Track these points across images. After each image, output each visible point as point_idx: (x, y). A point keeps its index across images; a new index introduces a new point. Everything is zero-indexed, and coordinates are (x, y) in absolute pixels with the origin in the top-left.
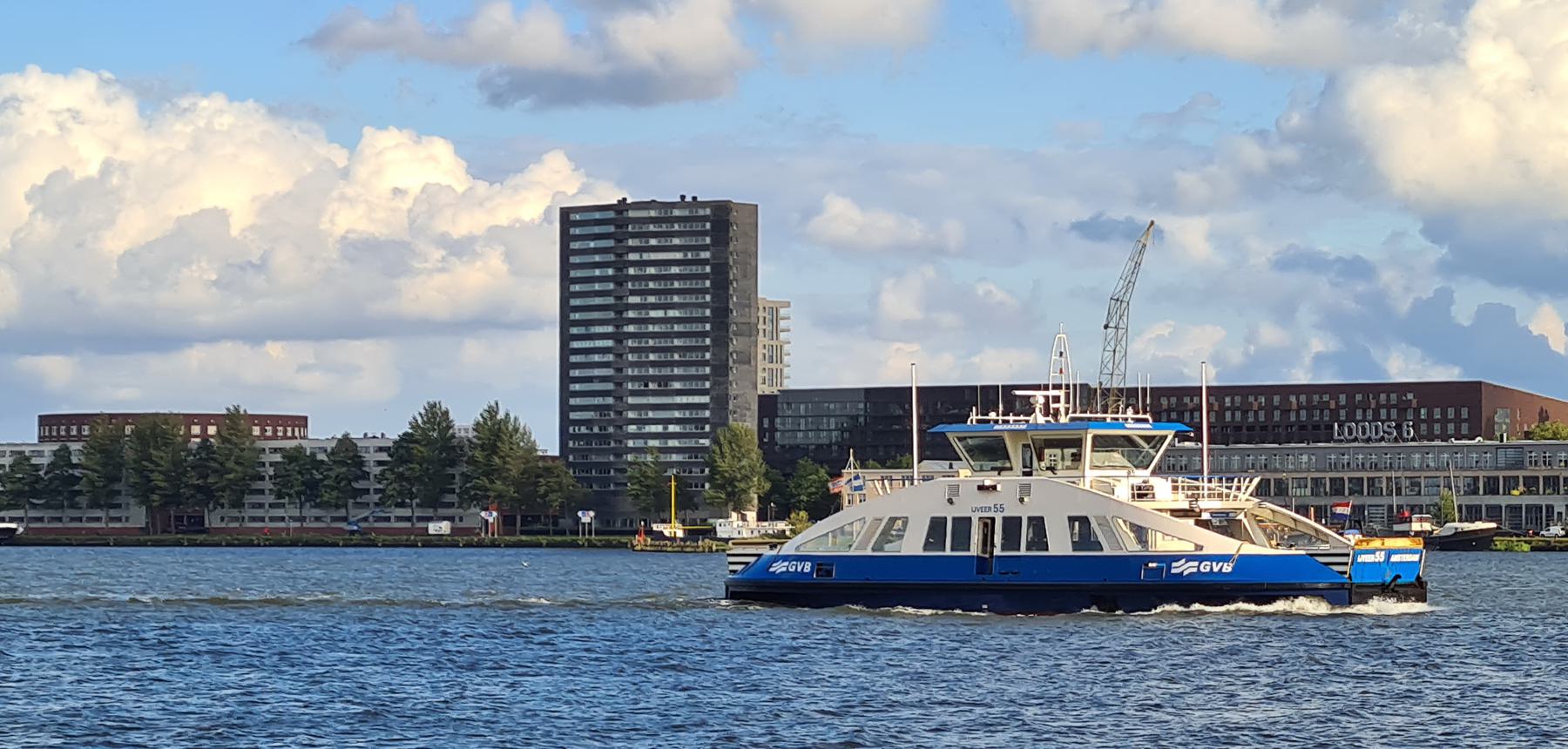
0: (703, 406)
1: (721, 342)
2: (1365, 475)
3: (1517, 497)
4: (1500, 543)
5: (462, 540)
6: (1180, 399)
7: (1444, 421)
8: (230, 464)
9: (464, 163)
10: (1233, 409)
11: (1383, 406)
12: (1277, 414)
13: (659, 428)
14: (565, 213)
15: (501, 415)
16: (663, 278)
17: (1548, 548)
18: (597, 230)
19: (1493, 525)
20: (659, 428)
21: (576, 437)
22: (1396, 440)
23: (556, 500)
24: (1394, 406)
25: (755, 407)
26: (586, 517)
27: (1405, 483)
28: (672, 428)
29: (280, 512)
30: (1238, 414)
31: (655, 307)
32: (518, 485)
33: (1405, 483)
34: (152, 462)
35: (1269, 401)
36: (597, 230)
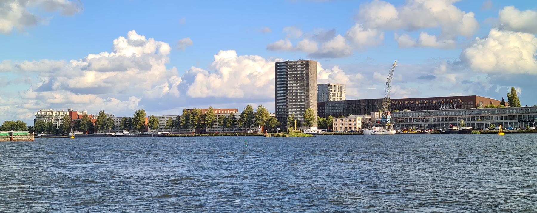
0: (304, 105)
1: (308, 91)
2: (445, 117)
3: (479, 121)
4: (473, 132)
5: (254, 134)
6: (446, 100)
7: (464, 105)
10: (421, 103)
16: (291, 76)
17: (484, 133)
18: (282, 67)
21: (279, 112)
23: (273, 125)
25: (316, 105)
26: (279, 129)
27: (454, 118)
28: (298, 110)
29: (220, 129)
31: (294, 84)
32: (266, 122)
33: (454, 118)
36: (282, 67)
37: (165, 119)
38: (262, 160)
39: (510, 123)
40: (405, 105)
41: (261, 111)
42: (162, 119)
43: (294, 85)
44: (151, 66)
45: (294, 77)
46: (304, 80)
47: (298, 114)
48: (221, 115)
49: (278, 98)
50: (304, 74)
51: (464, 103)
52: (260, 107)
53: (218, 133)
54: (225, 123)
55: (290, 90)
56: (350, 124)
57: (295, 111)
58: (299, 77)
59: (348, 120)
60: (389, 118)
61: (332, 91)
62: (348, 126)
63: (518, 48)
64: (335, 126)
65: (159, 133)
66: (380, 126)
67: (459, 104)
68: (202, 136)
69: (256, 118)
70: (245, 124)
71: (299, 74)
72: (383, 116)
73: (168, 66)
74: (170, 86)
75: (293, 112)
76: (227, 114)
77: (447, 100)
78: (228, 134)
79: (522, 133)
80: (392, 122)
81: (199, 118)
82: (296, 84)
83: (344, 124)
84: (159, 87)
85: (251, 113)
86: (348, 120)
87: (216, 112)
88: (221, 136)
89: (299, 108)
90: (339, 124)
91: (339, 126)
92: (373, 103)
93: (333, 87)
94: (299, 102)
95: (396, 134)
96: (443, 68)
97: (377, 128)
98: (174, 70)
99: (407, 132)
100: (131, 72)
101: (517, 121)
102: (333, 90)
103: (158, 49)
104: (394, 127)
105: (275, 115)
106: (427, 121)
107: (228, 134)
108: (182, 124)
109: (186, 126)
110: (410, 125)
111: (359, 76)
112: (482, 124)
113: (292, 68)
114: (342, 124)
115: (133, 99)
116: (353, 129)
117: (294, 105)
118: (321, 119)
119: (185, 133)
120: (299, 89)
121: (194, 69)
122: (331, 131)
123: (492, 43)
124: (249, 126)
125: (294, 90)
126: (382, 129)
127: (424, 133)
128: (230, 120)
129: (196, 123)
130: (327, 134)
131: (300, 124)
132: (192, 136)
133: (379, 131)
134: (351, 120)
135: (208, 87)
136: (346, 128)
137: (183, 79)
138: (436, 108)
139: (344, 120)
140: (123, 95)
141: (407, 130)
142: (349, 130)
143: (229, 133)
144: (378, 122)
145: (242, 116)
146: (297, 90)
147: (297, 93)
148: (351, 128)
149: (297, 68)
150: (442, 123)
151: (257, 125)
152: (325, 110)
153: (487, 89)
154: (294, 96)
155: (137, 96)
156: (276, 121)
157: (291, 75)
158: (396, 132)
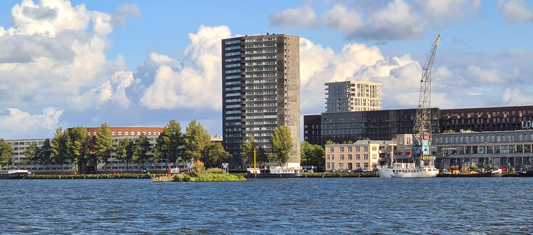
1: (281, 93)
8: (102, 146)
10: (496, 118)
11: (495, 117)
12: (514, 119)
13: (258, 129)
14: (224, 41)
15: (197, 125)
16: (253, 66)
18: (235, 48)
20: (258, 129)
21: (229, 133)
28: (263, 129)
29: (122, 165)
30: (498, 119)
31: (256, 79)
32: (202, 152)
34: (75, 146)
36: (235, 48)
37: (25, 146)
38: (113, 231)
40: (466, 120)
41: (194, 132)
42: (19, 146)
43: (256, 82)
44: (74, 54)
45: (255, 67)
46: (274, 72)
47: (263, 138)
48: (124, 138)
49: (227, 107)
50: (274, 60)
52: (193, 123)
53: (117, 172)
54: (130, 153)
55: (248, 91)
56: (358, 157)
57: (257, 132)
58: (265, 66)
59: (354, 148)
60: (426, 144)
61: (354, 95)
62: (354, 162)
64: (330, 161)
65: (10, 172)
68: (87, 178)
69: (186, 144)
70: (165, 156)
71: (265, 60)
72: (415, 141)
73: (110, 54)
74: (114, 87)
75: (253, 133)
76: (134, 136)
78: (134, 175)
80: (434, 153)
81: (83, 145)
82: (260, 79)
84: (96, 90)
85: (178, 134)
86: (354, 148)
87: (120, 133)
88: (122, 178)
89: (265, 126)
90: (336, 156)
92: (409, 118)
94: (266, 114)
95: (438, 176)
97: (403, 165)
98: (120, 60)
99: (457, 172)
100: (43, 63)
102: (356, 92)
103: (91, 23)
104: (438, 164)
105: (221, 139)
106: (498, 152)
107: (134, 175)
108: (52, 155)
109: (60, 160)
110: (467, 160)
113: (251, 50)
114: (343, 157)
115: (50, 111)
116: (362, 166)
117: (257, 120)
118: (312, 147)
119: (59, 173)
120: (265, 90)
121: (156, 57)
122: (323, 170)
124: (173, 160)
125: (256, 91)
126: (412, 166)
127: (489, 175)
128: (140, 148)
129: (78, 153)
130: (316, 177)
131: (266, 157)
132: (70, 178)
133: (406, 171)
135: (178, 92)
136: (350, 165)
137: (135, 77)
139: (346, 149)
140: (31, 103)
141: (460, 169)
142: (355, 168)
143: (136, 172)
144: (408, 153)
145: (160, 141)
146: (260, 91)
147: (262, 97)
148: (358, 165)
149: (261, 49)
150: (526, 155)
151: (187, 158)
152: (320, 129)
154: (256, 103)
155: (57, 106)
156: (221, 150)
157: (250, 62)
158: (437, 172)
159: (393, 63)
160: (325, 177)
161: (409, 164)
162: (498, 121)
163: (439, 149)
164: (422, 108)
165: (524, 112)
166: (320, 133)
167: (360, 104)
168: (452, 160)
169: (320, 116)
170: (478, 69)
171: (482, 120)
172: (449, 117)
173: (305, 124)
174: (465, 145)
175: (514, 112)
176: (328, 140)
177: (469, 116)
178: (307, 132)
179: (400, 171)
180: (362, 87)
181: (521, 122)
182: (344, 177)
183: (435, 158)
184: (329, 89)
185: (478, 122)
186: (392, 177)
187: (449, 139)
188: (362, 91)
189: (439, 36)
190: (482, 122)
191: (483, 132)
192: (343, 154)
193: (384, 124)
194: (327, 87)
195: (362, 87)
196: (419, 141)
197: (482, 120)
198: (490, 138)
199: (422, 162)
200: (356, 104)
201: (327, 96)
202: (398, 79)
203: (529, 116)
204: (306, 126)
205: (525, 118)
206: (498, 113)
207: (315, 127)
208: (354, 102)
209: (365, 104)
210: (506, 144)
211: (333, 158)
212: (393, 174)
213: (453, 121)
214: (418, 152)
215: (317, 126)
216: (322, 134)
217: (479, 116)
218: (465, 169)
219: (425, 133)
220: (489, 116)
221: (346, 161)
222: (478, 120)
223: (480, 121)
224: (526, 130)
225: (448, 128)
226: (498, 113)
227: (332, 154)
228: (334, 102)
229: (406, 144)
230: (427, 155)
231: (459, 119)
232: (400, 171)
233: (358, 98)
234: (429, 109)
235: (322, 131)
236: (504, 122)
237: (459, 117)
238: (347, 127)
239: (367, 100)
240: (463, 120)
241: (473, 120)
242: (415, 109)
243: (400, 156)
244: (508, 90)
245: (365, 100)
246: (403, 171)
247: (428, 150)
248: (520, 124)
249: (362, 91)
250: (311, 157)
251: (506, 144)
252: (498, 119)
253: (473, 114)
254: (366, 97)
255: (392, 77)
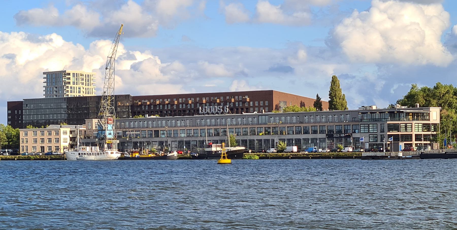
6: (225, 97)
7: (254, 107)
9: (71, 42)
10: (182, 104)
11: (181, 103)
19: (243, 148)
22: (222, 113)
24: (241, 101)
30: (184, 105)
35: (195, 99)
39: (313, 140)
40: (155, 106)
51: (254, 104)
56: (50, 140)
59: (46, 133)
61: (69, 83)
62: (46, 145)
63: (418, 24)
64: (24, 145)
66: (94, 144)
67: (246, 105)
77: (212, 98)
79: (328, 157)
83: (39, 141)
86: (46, 133)
91: (30, 144)
93: (71, 76)
95: (119, 159)
96: (302, 54)
97: (88, 148)
101: (324, 136)
102: (71, 81)
104: (121, 148)
110: (149, 143)
111: (177, 65)
112: (267, 141)
114: (36, 141)
116: (53, 149)
123: (377, 16)
127: (165, 157)
133: (91, 153)
134: (50, 134)
136: (43, 148)
138: (197, 112)
139: (39, 133)
142: (46, 151)
148: (50, 148)
152: (22, 115)
153: (378, 88)
158: (119, 155)
159: (132, 57)
160: (17, 160)
161: (93, 147)
162: (184, 107)
163: (124, 132)
164: (106, 94)
165: (207, 98)
166: (22, 118)
167: (75, 90)
168: (135, 143)
169: (22, 102)
170: (207, 63)
171: (169, 106)
172: (140, 103)
173: (8, 110)
174: (147, 129)
175: (198, 99)
176: (28, 125)
177: (158, 102)
178: (10, 117)
179: (85, 154)
180: (77, 76)
181: (199, 108)
182: (35, 159)
183: (118, 141)
184: (46, 78)
185: (166, 108)
186: (78, 159)
187: (134, 124)
188: (77, 80)
189: (122, 25)
190: (169, 108)
191: (166, 117)
192: (36, 137)
193: (80, 110)
194: (45, 76)
195: (77, 76)
196: (103, 125)
197: (169, 106)
198: (171, 122)
199: (106, 146)
200: (71, 92)
201: (45, 84)
202: (137, 72)
203: (211, 102)
204: (10, 112)
205: (208, 104)
206: (184, 99)
207: (18, 112)
208: (69, 89)
209: (79, 92)
210: (184, 128)
211: (27, 142)
212: (78, 156)
213: (143, 107)
214: (102, 136)
215: (20, 111)
216: (24, 119)
217: (167, 102)
218: (145, 153)
219: (109, 118)
220: (176, 102)
221: (39, 145)
222: (166, 106)
223: (168, 107)
224: (202, 116)
225: (139, 113)
226: (184, 99)
227: (26, 137)
228: (51, 90)
229: (94, 128)
230: (110, 139)
231: (148, 105)
232: (85, 154)
233: (73, 86)
234: (113, 96)
235: (24, 116)
236: (189, 107)
237: (148, 103)
238: (48, 113)
239: (82, 88)
240: (152, 106)
241: (161, 106)
242: (101, 96)
243: (89, 139)
244: (235, 82)
245: (80, 88)
246: (88, 154)
247: (112, 134)
248: (198, 110)
249: (77, 80)
250: (12, 141)
251: (184, 128)
252: (184, 105)
253: (161, 100)
254: (81, 85)
255: (132, 70)
